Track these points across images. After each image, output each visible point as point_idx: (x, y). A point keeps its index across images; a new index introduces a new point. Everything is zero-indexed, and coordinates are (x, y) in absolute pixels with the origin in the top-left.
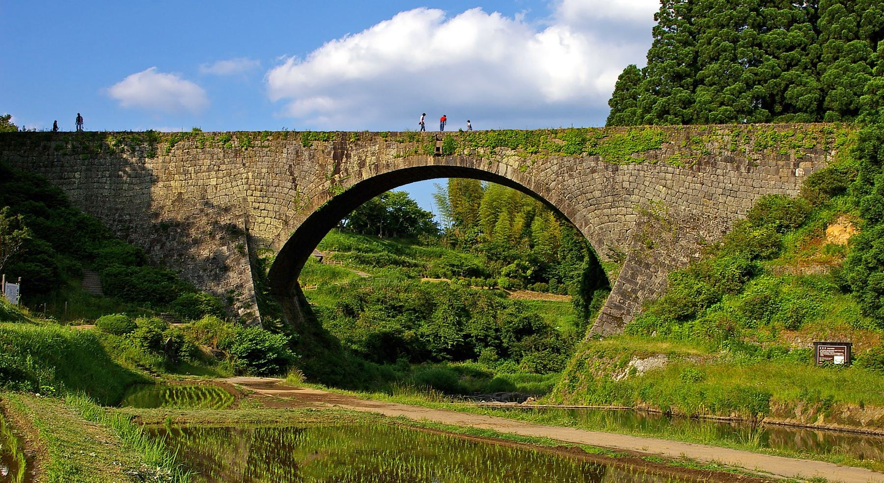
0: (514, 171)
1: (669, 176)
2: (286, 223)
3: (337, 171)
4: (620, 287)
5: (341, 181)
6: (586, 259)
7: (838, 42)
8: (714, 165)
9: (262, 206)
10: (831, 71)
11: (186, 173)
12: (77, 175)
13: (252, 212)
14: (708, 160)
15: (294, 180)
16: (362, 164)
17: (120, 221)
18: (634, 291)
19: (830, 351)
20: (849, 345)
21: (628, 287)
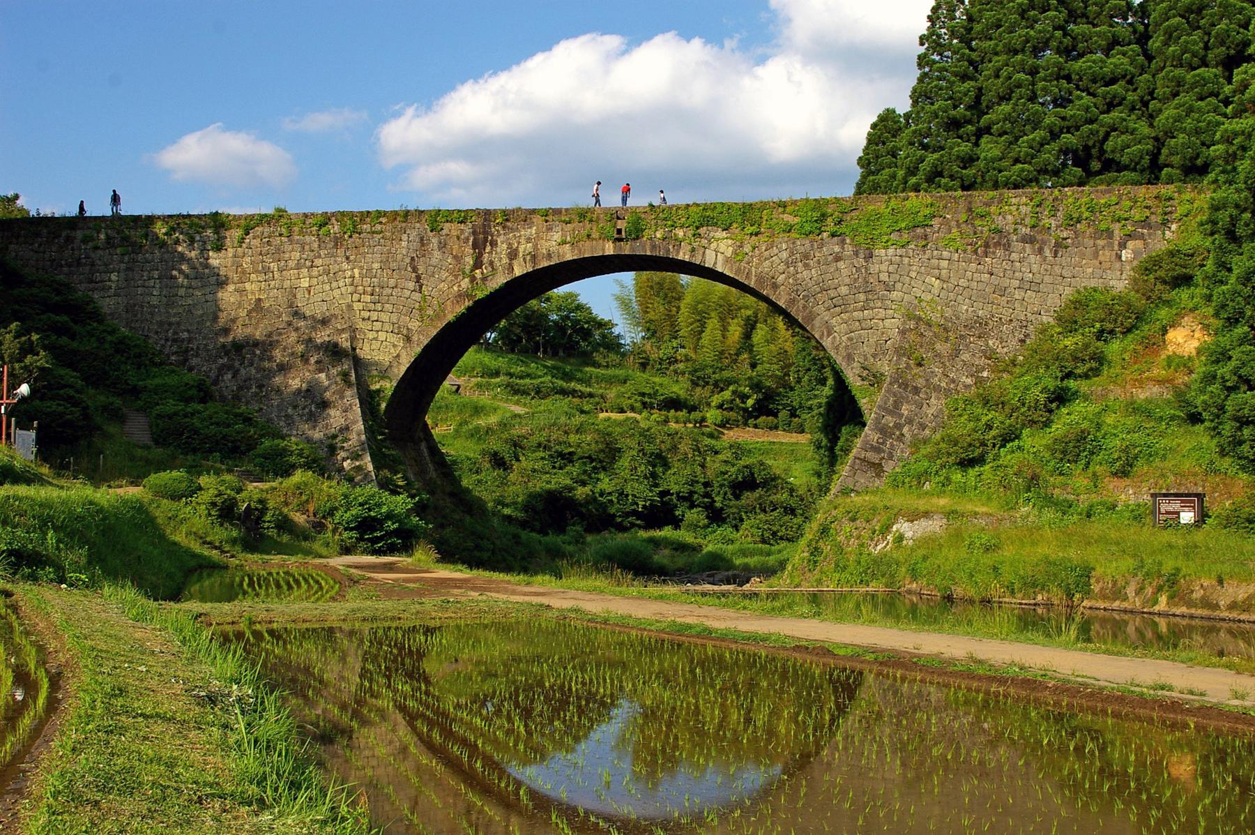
0: (727, 260)
1: (944, 264)
2: (408, 339)
3: (478, 264)
4: (877, 421)
5: (484, 279)
6: (830, 382)
7: (1178, 72)
8: (1007, 247)
9: (374, 316)
10: (1169, 112)
11: (266, 271)
12: (114, 277)
13: (361, 325)
14: (999, 240)
15: (418, 278)
16: (513, 255)
17: (175, 341)
18: (898, 426)
19: (1175, 506)
20: (1200, 497)
21: (890, 421)
